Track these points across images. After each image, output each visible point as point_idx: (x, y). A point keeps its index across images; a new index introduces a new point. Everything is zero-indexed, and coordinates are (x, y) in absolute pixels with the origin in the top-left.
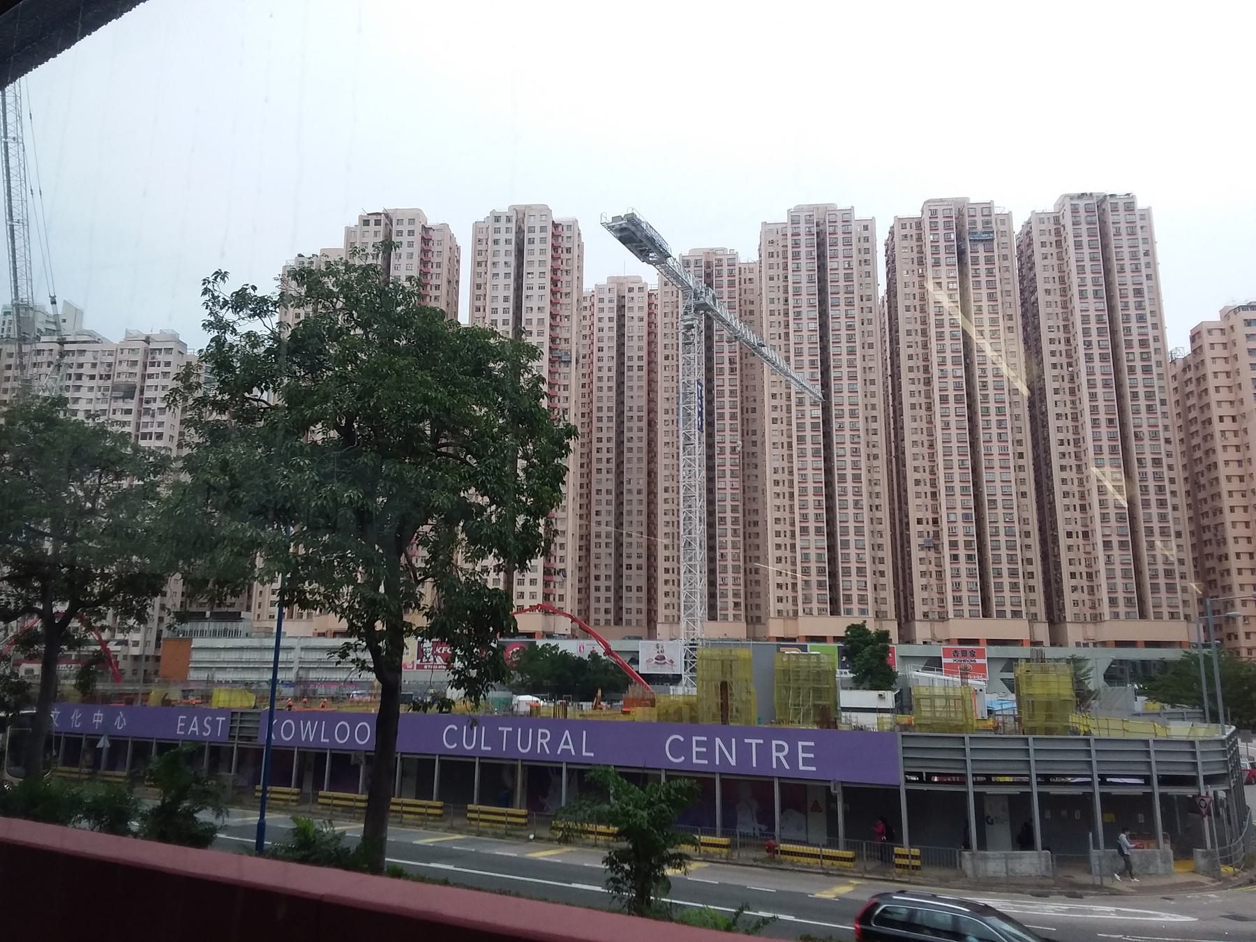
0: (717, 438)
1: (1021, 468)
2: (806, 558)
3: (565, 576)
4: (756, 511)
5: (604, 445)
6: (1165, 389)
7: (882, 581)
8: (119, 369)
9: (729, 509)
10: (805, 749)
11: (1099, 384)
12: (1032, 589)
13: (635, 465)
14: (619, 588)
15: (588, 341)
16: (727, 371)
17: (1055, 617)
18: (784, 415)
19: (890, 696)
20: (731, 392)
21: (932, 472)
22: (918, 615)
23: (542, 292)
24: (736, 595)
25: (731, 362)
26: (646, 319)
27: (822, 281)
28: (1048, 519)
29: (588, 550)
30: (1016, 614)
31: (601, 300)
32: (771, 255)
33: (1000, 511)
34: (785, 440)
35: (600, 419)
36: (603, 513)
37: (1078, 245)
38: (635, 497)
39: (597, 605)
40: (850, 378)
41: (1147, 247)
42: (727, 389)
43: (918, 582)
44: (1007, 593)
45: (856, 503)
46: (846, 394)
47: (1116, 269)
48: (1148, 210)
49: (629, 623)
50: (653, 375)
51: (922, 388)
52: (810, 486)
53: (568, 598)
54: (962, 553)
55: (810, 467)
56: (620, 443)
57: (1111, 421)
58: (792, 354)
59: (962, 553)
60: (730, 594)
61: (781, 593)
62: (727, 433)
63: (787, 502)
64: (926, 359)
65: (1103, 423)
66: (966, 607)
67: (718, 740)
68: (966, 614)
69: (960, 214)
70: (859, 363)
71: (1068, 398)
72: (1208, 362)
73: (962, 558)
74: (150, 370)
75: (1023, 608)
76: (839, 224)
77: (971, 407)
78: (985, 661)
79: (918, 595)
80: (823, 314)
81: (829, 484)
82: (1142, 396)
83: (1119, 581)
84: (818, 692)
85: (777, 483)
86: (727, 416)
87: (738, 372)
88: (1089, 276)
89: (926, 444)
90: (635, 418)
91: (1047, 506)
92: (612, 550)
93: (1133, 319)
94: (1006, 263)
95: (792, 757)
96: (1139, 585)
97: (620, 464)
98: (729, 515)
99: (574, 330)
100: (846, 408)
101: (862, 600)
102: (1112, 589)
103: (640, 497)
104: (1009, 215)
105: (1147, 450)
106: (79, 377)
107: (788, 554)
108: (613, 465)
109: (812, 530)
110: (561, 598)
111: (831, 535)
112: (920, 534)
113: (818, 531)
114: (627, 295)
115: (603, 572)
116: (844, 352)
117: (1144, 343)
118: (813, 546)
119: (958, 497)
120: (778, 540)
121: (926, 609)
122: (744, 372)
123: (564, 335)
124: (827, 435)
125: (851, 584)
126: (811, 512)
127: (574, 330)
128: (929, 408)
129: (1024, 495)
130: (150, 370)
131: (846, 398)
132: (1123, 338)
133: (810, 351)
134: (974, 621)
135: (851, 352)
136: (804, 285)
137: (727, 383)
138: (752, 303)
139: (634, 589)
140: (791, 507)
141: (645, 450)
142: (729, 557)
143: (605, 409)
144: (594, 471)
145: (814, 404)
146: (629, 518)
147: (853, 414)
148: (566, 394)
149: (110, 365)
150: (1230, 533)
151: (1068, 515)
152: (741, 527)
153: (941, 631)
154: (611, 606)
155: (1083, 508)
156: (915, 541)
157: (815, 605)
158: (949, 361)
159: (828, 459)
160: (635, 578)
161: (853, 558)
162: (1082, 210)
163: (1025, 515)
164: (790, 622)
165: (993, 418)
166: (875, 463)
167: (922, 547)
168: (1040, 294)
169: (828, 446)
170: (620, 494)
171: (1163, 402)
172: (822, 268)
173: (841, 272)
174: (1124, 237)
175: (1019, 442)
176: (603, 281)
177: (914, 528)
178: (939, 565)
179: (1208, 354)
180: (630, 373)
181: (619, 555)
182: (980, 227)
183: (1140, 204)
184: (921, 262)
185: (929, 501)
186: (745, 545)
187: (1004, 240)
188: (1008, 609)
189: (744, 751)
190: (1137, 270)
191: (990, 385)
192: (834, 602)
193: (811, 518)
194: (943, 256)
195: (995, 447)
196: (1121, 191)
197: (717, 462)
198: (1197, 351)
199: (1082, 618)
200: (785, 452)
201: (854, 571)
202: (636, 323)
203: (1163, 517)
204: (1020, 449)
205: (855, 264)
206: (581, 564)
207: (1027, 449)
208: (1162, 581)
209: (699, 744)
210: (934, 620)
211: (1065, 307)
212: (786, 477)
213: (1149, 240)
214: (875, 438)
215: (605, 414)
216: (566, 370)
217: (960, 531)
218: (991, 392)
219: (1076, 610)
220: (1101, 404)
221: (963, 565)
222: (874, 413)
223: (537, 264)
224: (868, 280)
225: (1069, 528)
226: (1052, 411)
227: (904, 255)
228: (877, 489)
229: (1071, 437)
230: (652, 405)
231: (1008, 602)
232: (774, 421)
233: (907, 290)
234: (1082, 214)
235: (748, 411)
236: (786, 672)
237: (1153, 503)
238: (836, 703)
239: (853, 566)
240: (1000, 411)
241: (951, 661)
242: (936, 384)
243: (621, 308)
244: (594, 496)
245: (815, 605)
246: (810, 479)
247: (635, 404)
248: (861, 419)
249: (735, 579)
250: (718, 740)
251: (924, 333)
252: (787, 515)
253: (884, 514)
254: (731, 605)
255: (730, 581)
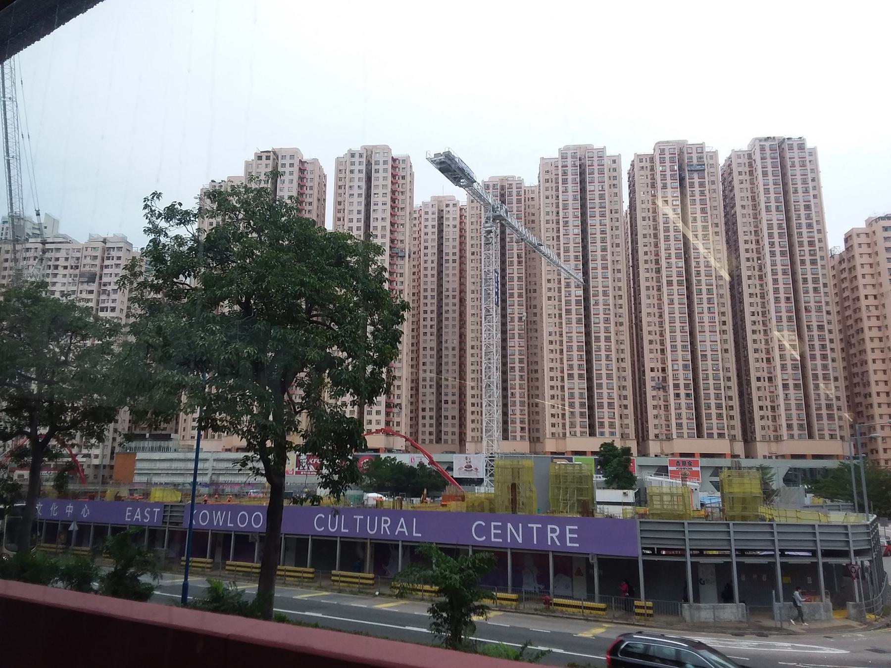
0: (509, 311)
1: (724, 332)
2: (572, 396)
3: (401, 409)
4: (537, 363)
5: (429, 316)
6: (826, 276)
7: (626, 412)
8: (84, 262)
9: (517, 361)
10: (571, 531)
11: (780, 272)
12: (732, 418)
13: (450, 330)
14: (439, 417)
15: (417, 242)
16: (516, 263)
17: (748, 437)
18: (556, 294)
19: (631, 493)
20: (519, 278)
21: (661, 335)
22: (651, 436)
23: (384, 207)
24: (522, 422)
25: (519, 256)
26: (458, 226)
27: (583, 199)
28: (744, 368)
29: (417, 390)
30: (721, 436)
31: (427, 213)
32: (547, 181)
33: (710, 362)
34: (557, 312)
35: (426, 297)
36: (428, 364)
37: (765, 174)
38: (451, 353)
39: (424, 429)
40: (603, 268)
41: (813, 175)
42: (516, 276)
43: (651, 413)
44: (714, 421)
45: (607, 357)
46: (600, 279)
47: (791, 190)
48: (815, 149)
49: (446, 441)
50: (463, 266)
51: (654, 275)
52: (575, 345)
53: (403, 424)
54: (682, 392)
55: (574, 331)
56: (440, 314)
57: (788, 299)
58: (562, 251)
59: (682, 392)
60: (518, 421)
61: (554, 420)
62: (516, 307)
63: (558, 356)
64: (657, 255)
65: (783, 300)
66: (685, 431)
67: (509, 525)
68: (686, 436)
69: (681, 152)
70: (609, 257)
71: (757, 282)
72: (857, 256)
73: (683, 396)
74: (107, 263)
75: (726, 431)
76: (596, 159)
77: (689, 288)
78: (699, 469)
79: (652, 422)
80: (584, 223)
81: (588, 343)
82: (810, 281)
83: (794, 412)
84: (580, 491)
85: (551, 342)
86: (516, 295)
87: (523, 264)
88: (772, 196)
89: (657, 315)
90: (451, 297)
91: (743, 359)
92: (434, 390)
93: (804, 226)
94: (713, 187)
95: (562, 537)
96: (808, 415)
97: (440, 329)
98: (517, 365)
99: (407, 234)
100: (600, 289)
101: (612, 425)
102: (789, 418)
103: (454, 352)
104: (716, 153)
105: (814, 319)
106: (56, 267)
107: (559, 393)
108: (435, 330)
109: (576, 376)
110: (398, 424)
111: (590, 380)
112: (653, 379)
113: (581, 376)
114: (445, 209)
115: (428, 406)
116: (599, 249)
117: (811, 243)
118: (576, 387)
119: (680, 352)
120: (552, 383)
121: (657, 432)
122: (528, 264)
123: (400, 237)
124: (587, 309)
125: (603, 414)
126: (575, 363)
127: (407, 234)
128: (659, 290)
129: (726, 351)
130: (107, 263)
131: (600, 282)
132: (797, 240)
133: (574, 249)
134: (691, 441)
135: (604, 249)
136: (570, 202)
137: (516, 271)
138: (533, 215)
139: (450, 418)
140: (561, 359)
141: (457, 319)
142: (517, 395)
143: (429, 290)
144: (421, 334)
145: (578, 287)
146: (446, 368)
147: (605, 294)
148: (402, 279)
149: (78, 259)
150: (873, 378)
151: (758, 365)
152: (525, 374)
153: (668, 447)
154: (433, 429)
155: (768, 360)
156: (649, 384)
157: (578, 429)
158: (673, 256)
159: (587, 326)
160: (450, 410)
161: (605, 396)
162: (767, 149)
163: (727, 365)
164: (560, 441)
165: (705, 296)
166: (621, 328)
167: (654, 388)
168: (738, 208)
169: (587, 316)
170: (440, 350)
171: (825, 285)
172: (583, 190)
173: (597, 193)
174: (798, 168)
175: (723, 314)
176: (428, 199)
177: (648, 375)
178: (666, 401)
179: (857, 251)
180: (447, 265)
181: (439, 394)
182: (695, 161)
183: (809, 145)
184: (653, 186)
185: (659, 355)
186: (528, 386)
187: (712, 170)
188: (715, 432)
189: (528, 533)
190: (806, 191)
191: (703, 273)
192: (592, 427)
193: (576, 367)
194: (669, 181)
195: (706, 317)
196: (795, 136)
197: (509, 327)
198: (849, 249)
199: (768, 438)
200: (557, 320)
201: (606, 405)
202: (451, 229)
203: (825, 367)
204: (723, 319)
205: (606, 187)
206: (412, 400)
207: (729, 318)
208: (824, 412)
209: (496, 527)
210: (662, 440)
211: (755, 217)
212: (558, 338)
213: (815, 170)
214: (621, 311)
215: (429, 293)
216: (402, 262)
217: (681, 377)
218: (703, 278)
219: (763, 432)
220: (781, 286)
221: (683, 401)
222: (620, 293)
223: (381, 187)
224: (616, 199)
225: (758, 374)
226: (746, 292)
227: (641, 181)
228: (622, 347)
229: (760, 310)
230: (463, 287)
231: (715, 427)
232: (549, 298)
233: (644, 206)
234: (768, 152)
235: (531, 291)
236: (557, 476)
237: (818, 357)
238: (593, 498)
239: (605, 401)
240: (709, 292)
241: (674, 468)
242: (664, 272)
243: (441, 218)
244: (421, 352)
245: (578, 429)
246: (575, 339)
247: (451, 286)
248: (611, 297)
249: (521, 411)
250: (509, 525)
251: (656, 236)
252: (558, 365)
253: (627, 365)
254: (519, 429)
255: (518, 412)
